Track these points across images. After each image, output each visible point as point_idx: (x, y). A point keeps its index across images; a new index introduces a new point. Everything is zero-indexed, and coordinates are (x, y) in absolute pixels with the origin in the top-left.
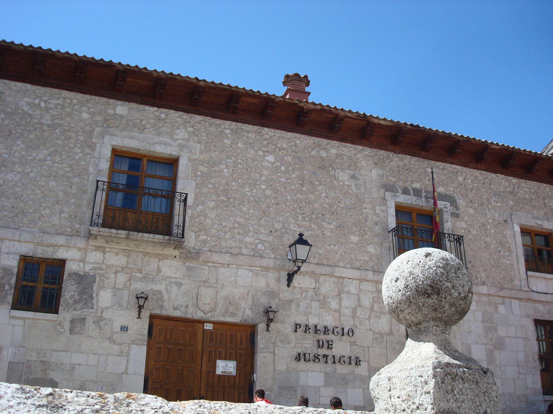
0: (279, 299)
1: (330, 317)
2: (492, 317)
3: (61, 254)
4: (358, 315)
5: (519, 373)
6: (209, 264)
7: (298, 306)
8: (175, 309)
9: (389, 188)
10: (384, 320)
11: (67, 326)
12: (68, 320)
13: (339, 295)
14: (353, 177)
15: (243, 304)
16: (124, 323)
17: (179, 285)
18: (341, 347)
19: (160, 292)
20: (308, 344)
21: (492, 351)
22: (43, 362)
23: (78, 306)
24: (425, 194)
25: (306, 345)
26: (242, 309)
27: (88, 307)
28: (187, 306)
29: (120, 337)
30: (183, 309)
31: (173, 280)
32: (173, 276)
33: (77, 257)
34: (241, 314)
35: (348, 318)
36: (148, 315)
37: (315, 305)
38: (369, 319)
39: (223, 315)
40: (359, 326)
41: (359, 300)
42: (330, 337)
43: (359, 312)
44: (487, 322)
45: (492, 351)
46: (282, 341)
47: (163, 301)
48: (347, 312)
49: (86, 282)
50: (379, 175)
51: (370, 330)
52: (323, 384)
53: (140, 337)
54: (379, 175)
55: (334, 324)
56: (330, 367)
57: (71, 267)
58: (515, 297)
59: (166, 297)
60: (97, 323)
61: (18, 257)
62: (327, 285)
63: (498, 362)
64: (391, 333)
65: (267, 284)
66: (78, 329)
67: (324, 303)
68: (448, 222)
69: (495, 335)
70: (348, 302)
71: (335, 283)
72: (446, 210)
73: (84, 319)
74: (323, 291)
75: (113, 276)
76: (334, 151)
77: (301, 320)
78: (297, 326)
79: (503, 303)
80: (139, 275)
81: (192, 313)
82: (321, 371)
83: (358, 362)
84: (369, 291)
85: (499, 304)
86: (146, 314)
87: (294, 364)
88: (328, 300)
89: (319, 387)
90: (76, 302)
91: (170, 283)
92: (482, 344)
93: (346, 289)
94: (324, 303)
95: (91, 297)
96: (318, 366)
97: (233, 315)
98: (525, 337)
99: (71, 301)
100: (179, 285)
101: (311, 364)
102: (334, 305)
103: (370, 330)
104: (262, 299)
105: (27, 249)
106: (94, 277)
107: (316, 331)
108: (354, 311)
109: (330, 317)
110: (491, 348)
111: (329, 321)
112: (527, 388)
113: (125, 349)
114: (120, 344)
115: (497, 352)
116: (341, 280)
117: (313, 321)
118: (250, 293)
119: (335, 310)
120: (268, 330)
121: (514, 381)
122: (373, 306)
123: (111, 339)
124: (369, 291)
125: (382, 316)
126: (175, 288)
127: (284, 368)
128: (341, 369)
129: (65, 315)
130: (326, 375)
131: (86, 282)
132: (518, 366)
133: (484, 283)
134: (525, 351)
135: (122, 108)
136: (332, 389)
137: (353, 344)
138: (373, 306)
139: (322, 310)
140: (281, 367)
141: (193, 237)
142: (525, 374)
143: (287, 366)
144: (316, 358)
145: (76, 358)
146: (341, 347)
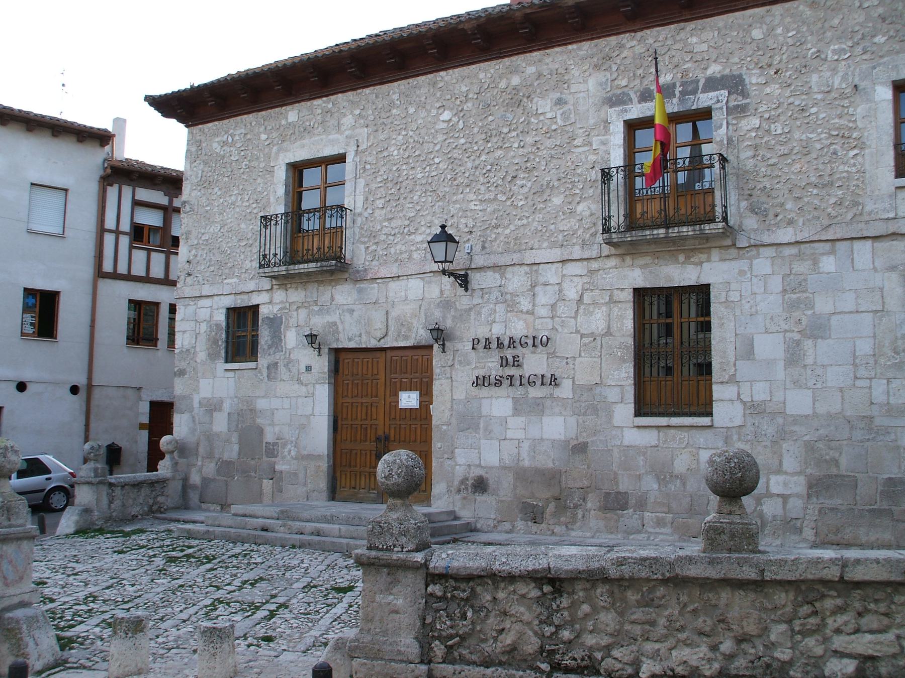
0: (456, 309)
1: (521, 322)
2: (805, 280)
3: (255, 300)
4: (558, 313)
5: (856, 378)
6: (378, 281)
7: (479, 313)
8: (350, 340)
9: (617, 100)
10: (599, 315)
11: (265, 372)
12: (265, 365)
13: (533, 287)
14: (560, 102)
15: (415, 322)
16: (308, 363)
17: (351, 311)
18: (534, 363)
19: (335, 324)
20: (491, 365)
21: (798, 343)
22: (251, 410)
23: (272, 351)
24: (680, 89)
25: (490, 365)
26: (415, 330)
27: (279, 351)
28: (360, 335)
29: (305, 377)
30: (357, 339)
31: (346, 307)
32: (345, 302)
33: (270, 302)
34: (414, 336)
35: (545, 320)
36: (327, 350)
37: (500, 308)
38: (575, 318)
39: (396, 340)
40: (560, 330)
41: (560, 291)
42: (519, 351)
43: (561, 309)
44: (793, 291)
45: (798, 343)
46: (460, 362)
47: (338, 333)
48: (543, 312)
49: (275, 322)
50: (601, 84)
51: (577, 332)
52: (511, 414)
53: (321, 375)
54: (601, 84)
55: (525, 332)
56: (519, 392)
57: (264, 311)
58: (859, 235)
59: (340, 328)
60: (286, 366)
61: (224, 311)
62: (516, 279)
63: (809, 361)
64: (608, 333)
65: (441, 291)
66: (273, 374)
67: (511, 305)
68: (721, 127)
69: (809, 312)
70: (544, 298)
71: (526, 273)
72: (719, 105)
73: (277, 363)
74: (510, 288)
75: (295, 313)
76: (531, 70)
77: (482, 332)
78: (475, 342)
79: (832, 252)
80: (316, 308)
81: (365, 343)
82: (509, 396)
83: (554, 381)
84: (576, 276)
85: (823, 254)
86: (325, 351)
87: (475, 391)
88: (517, 299)
89: (506, 418)
90: (270, 347)
91: (343, 311)
92: (777, 332)
93: (542, 280)
94: (511, 305)
95: (281, 340)
96: (504, 390)
97: (406, 338)
98: (880, 308)
99: (266, 347)
100: (351, 311)
101: (495, 391)
102: (525, 304)
103: (577, 332)
104: (436, 313)
105: (229, 302)
106: (281, 318)
107: (500, 345)
108: (553, 307)
109: (521, 322)
110: (797, 336)
111: (518, 328)
112: (872, 403)
113: (310, 388)
114: (306, 385)
115: (808, 344)
116: (535, 268)
117: (497, 330)
118: (423, 307)
119: (527, 312)
120: (444, 351)
121: (841, 391)
122: (581, 296)
123: (299, 382)
124: (576, 276)
125: (597, 311)
126: (347, 316)
127: (463, 397)
128: (535, 392)
129: (263, 361)
130: (516, 401)
131: (275, 322)
132: (855, 365)
133: (791, 222)
134: (874, 337)
135: (292, 114)
136: (523, 419)
137: (552, 355)
138: (581, 296)
139: (509, 314)
140: (460, 395)
141: (363, 250)
142: (870, 379)
143: (467, 393)
144: (499, 383)
145: (275, 403)
146: (534, 363)
